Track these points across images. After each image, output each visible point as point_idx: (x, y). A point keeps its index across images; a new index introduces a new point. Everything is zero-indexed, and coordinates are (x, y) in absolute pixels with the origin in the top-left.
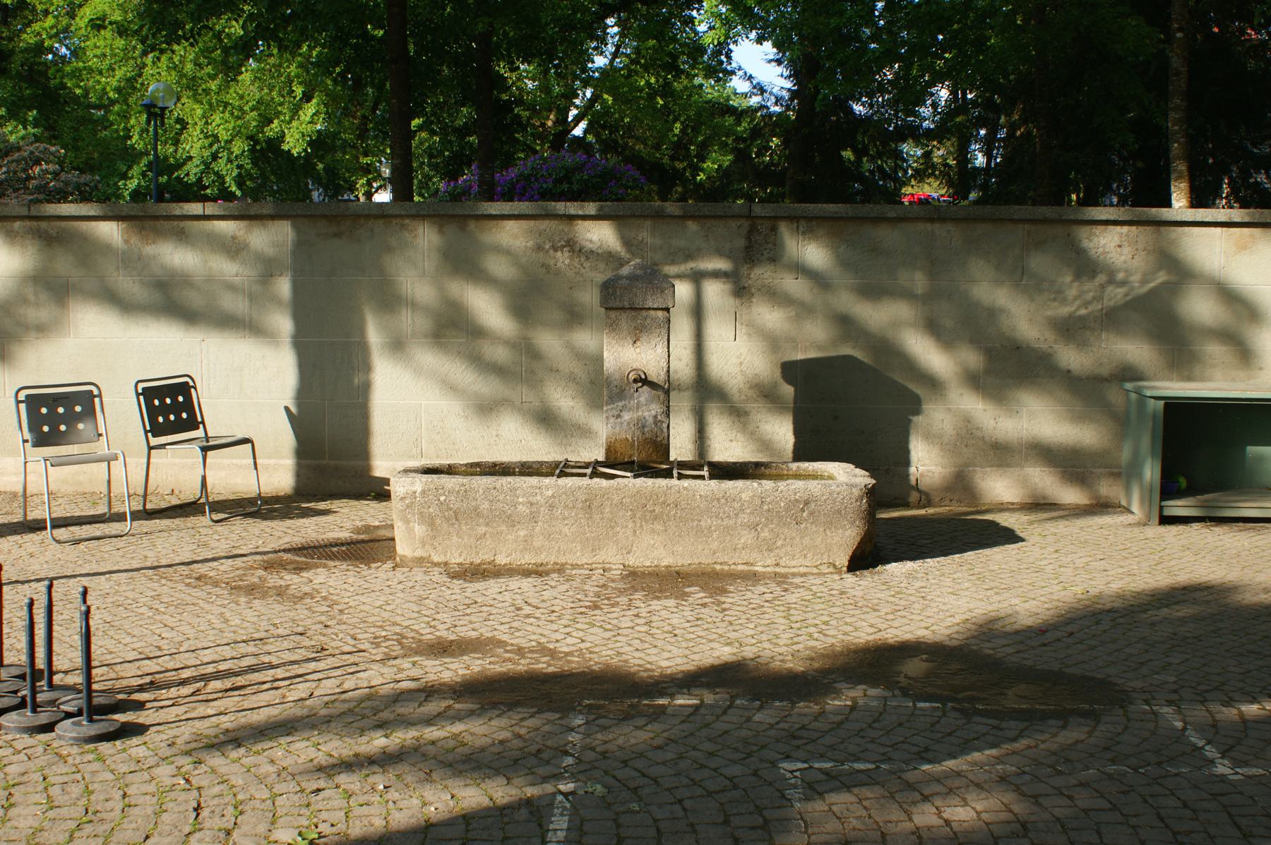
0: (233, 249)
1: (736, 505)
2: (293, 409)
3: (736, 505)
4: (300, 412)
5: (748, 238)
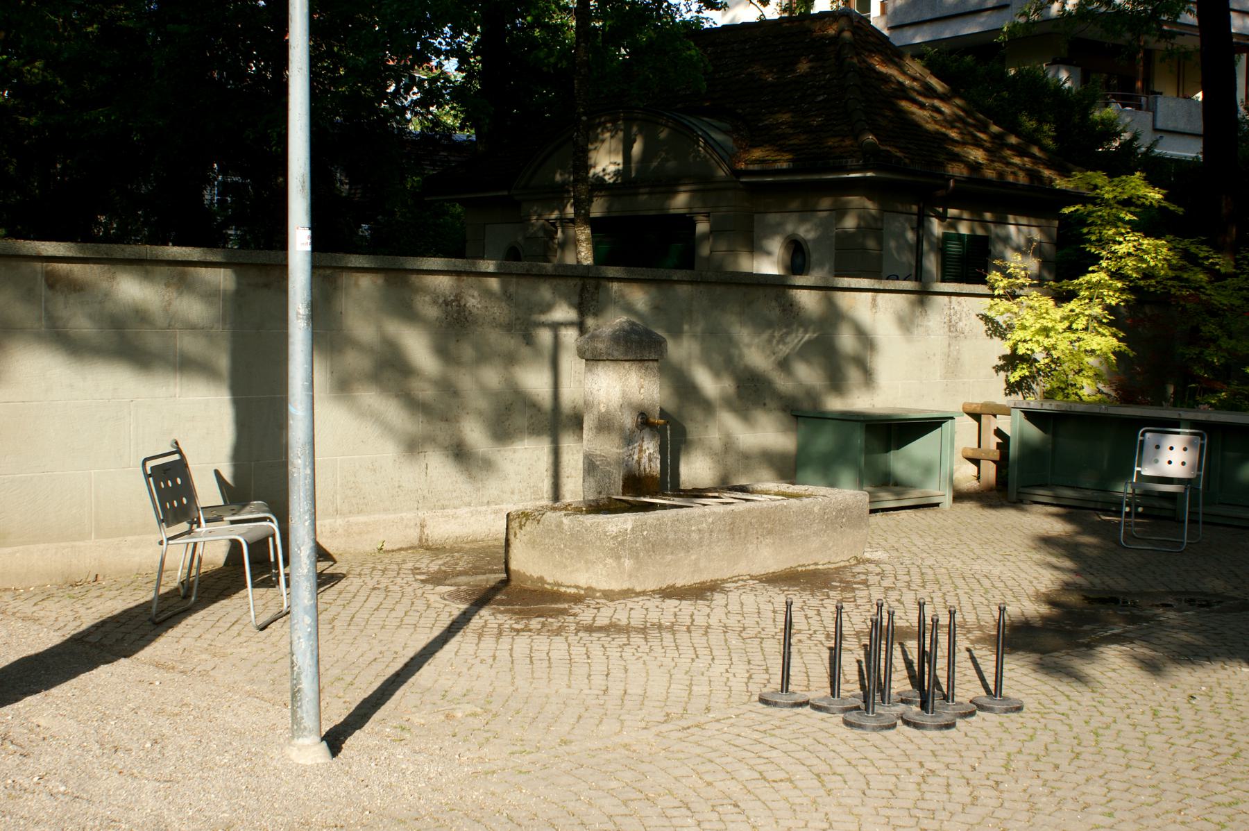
2: (227, 474)
4: (236, 476)
5: (581, 296)
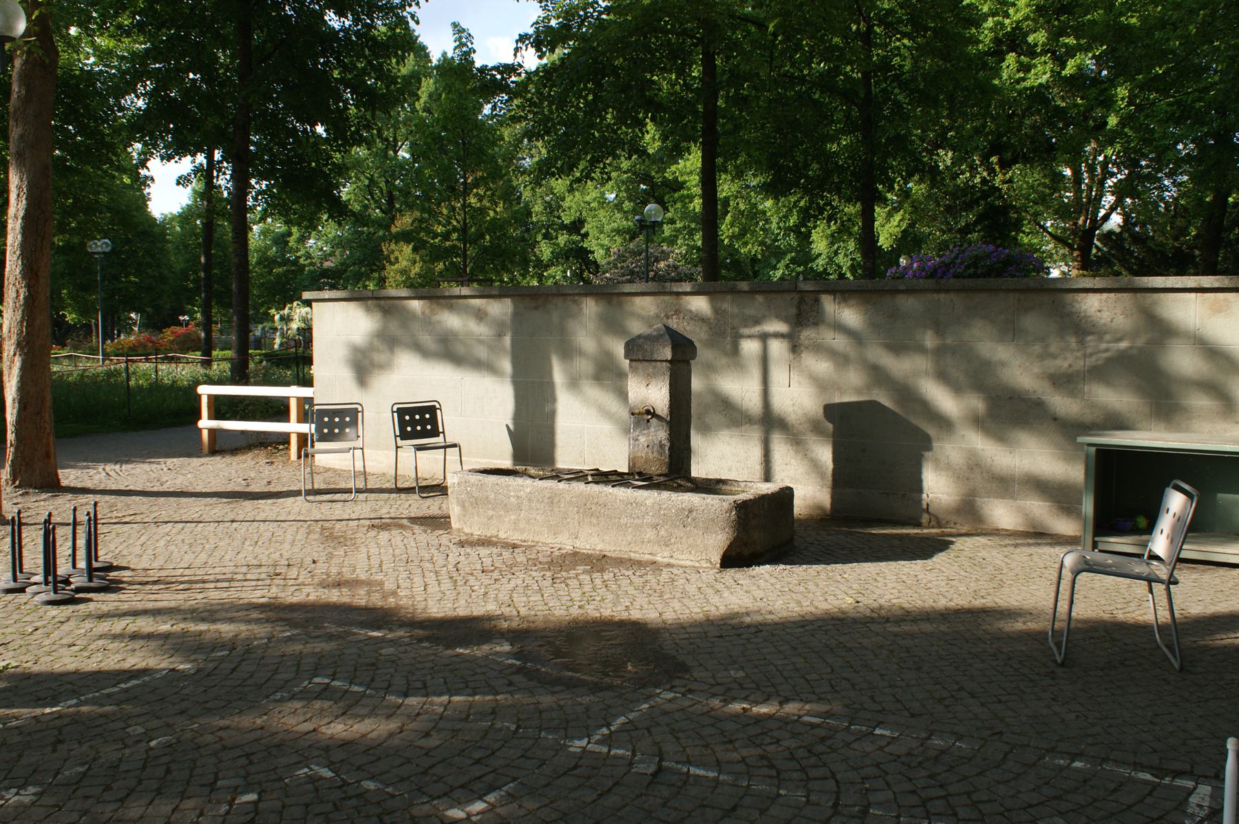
0: (480, 315)
1: (643, 509)
2: (511, 427)
3: (643, 509)
5: (799, 308)
